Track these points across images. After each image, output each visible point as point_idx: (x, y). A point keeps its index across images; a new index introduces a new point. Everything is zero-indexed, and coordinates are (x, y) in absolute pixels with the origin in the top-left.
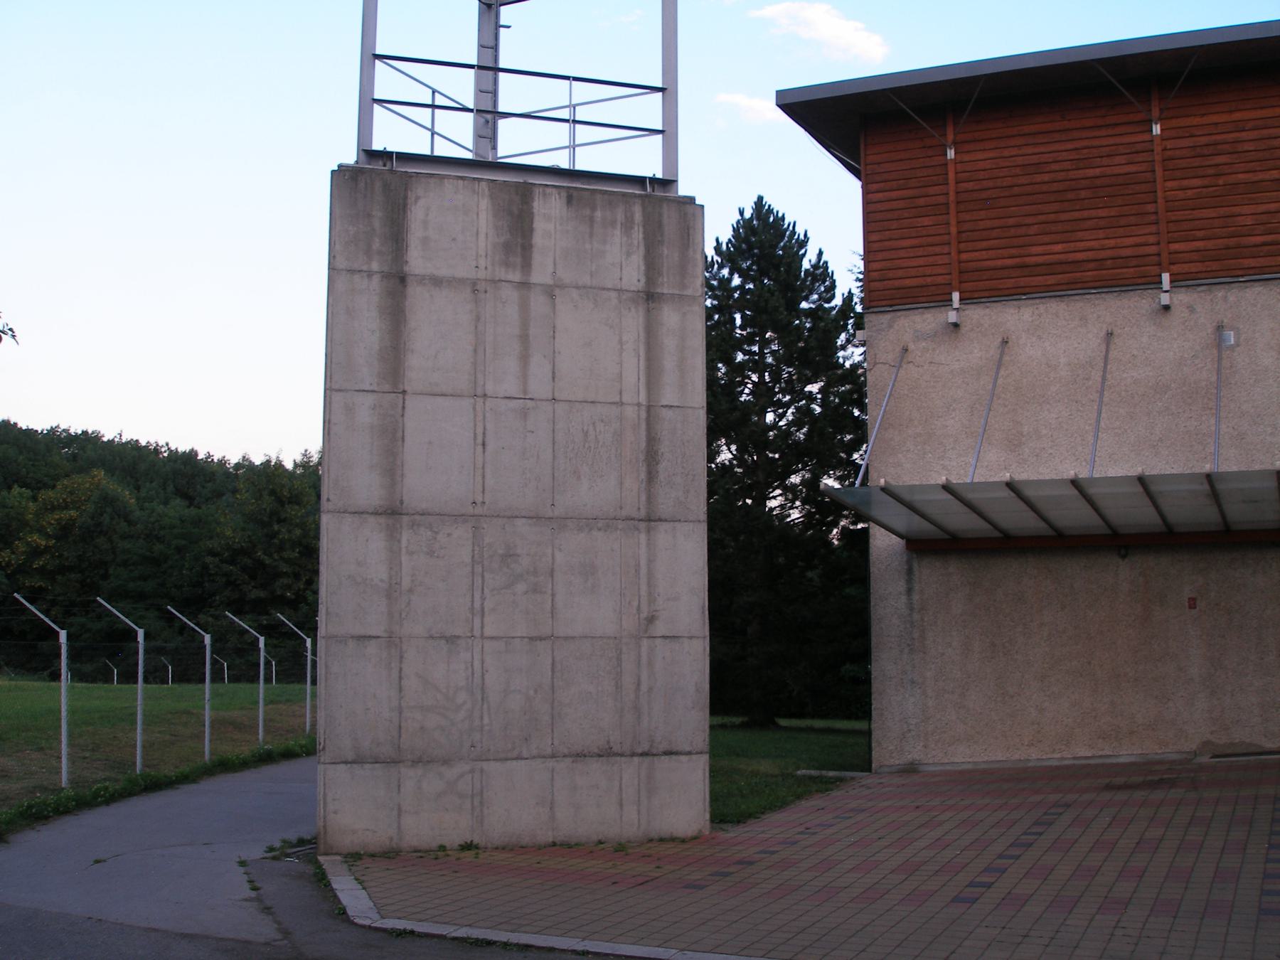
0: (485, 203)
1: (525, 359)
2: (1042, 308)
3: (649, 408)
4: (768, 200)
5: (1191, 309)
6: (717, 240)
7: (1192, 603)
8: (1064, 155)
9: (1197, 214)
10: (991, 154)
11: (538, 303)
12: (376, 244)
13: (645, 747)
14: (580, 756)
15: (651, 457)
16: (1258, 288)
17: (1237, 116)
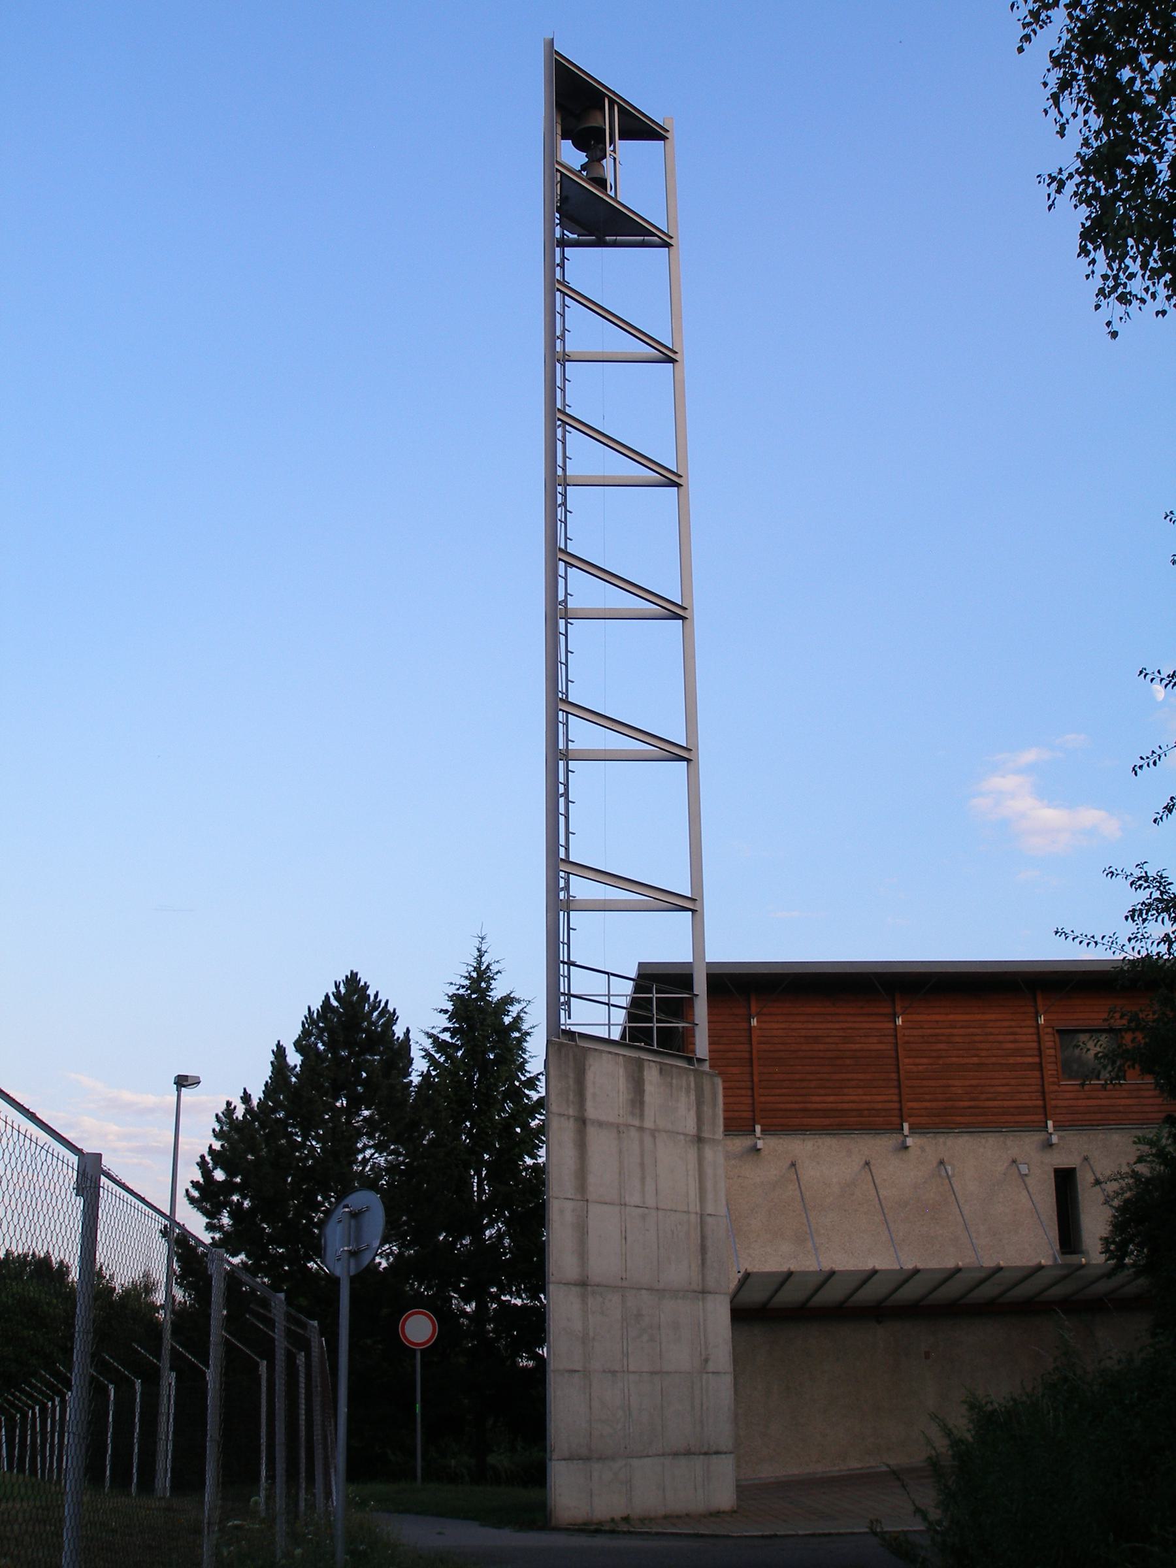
0: (621, 1071)
1: (643, 1179)
2: (820, 1141)
3: (702, 1215)
4: (364, 978)
5: (923, 1150)
6: (309, 1009)
7: (927, 1355)
8: (835, 1033)
9: (925, 1083)
10: (783, 1026)
11: (648, 1140)
12: (571, 1097)
13: (705, 1449)
14: (676, 1454)
15: (703, 1249)
16: (966, 1138)
17: (951, 1017)
